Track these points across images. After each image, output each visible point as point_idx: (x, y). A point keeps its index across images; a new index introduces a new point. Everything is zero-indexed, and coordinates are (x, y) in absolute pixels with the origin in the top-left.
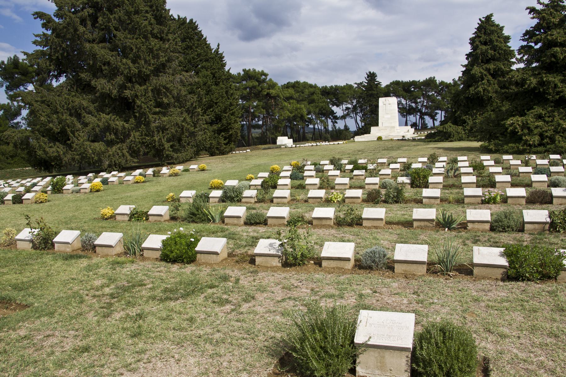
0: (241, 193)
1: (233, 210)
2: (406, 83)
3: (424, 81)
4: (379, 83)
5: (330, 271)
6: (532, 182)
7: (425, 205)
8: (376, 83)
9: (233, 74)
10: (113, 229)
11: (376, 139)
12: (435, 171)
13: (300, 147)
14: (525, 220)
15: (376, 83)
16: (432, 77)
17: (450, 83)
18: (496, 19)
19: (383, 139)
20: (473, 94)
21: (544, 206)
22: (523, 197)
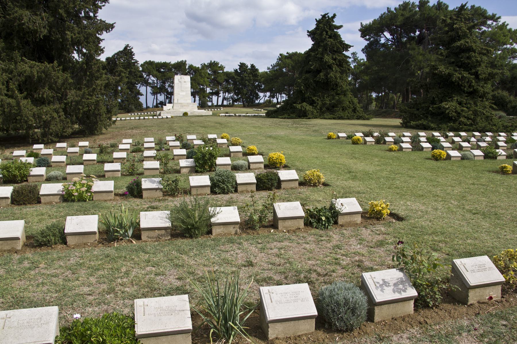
0: (27, 170)
1: (242, 177)
2: (158, 64)
3: (174, 64)
4: (137, 62)
5: (77, 246)
6: (231, 152)
7: (251, 169)
8: (133, 61)
9: (343, 40)
10: (7, 218)
11: (182, 115)
12: (121, 147)
13: (125, 120)
14: (238, 182)
15: (133, 61)
16: (184, 60)
17: (199, 67)
18: (337, 22)
19: (189, 115)
20: (323, 78)
21: (12, 184)
22: (229, 165)
